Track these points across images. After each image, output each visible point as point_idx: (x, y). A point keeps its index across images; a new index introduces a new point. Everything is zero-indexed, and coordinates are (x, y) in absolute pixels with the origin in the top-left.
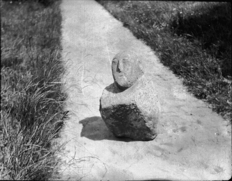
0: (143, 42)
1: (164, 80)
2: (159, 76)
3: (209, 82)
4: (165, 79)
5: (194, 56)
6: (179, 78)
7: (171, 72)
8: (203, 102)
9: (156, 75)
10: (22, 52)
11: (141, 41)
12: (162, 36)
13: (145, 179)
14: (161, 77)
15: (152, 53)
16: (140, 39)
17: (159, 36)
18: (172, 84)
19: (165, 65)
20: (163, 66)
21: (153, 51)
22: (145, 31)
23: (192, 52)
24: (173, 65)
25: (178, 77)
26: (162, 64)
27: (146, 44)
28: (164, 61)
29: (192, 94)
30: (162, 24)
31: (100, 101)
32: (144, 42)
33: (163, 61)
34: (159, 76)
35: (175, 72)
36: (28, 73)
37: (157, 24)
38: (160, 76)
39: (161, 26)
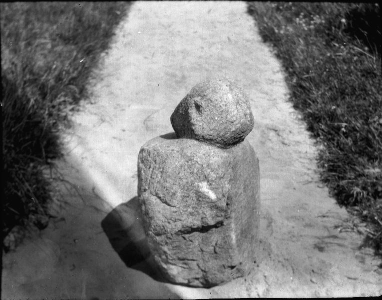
0: (272, 49)
1: (283, 143)
2: (276, 131)
3: (374, 168)
4: (286, 141)
5: (357, 97)
6: (316, 144)
7: (304, 125)
8: (346, 212)
9: (271, 129)
10: (246, 265)
11: (269, 46)
12: (307, 44)
13: (176, 1)
14: (278, 135)
15: (280, 76)
16: (268, 44)
17: (302, 42)
18: (295, 156)
19: (296, 107)
20: (292, 110)
21: (284, 73)
22: (279, 27)
23: (354, 89)
24: (309, 112)
25: (314, 141)
26: (291, 104)
27: (275, 54)
28: (296, 98)
29: (326, 189)
30: (315, 18)
31: (349, 278)
32: (274, 50)
33: (294, 99)
34: (276, 131)
35: (311, 128)
36: (65, 81)
37: (305, 17)
38: (277, 132)
39: (312, 22)
